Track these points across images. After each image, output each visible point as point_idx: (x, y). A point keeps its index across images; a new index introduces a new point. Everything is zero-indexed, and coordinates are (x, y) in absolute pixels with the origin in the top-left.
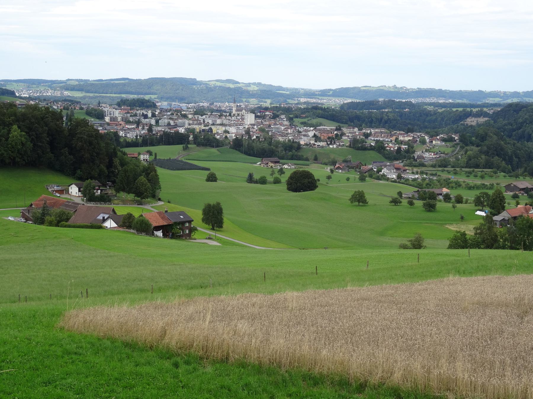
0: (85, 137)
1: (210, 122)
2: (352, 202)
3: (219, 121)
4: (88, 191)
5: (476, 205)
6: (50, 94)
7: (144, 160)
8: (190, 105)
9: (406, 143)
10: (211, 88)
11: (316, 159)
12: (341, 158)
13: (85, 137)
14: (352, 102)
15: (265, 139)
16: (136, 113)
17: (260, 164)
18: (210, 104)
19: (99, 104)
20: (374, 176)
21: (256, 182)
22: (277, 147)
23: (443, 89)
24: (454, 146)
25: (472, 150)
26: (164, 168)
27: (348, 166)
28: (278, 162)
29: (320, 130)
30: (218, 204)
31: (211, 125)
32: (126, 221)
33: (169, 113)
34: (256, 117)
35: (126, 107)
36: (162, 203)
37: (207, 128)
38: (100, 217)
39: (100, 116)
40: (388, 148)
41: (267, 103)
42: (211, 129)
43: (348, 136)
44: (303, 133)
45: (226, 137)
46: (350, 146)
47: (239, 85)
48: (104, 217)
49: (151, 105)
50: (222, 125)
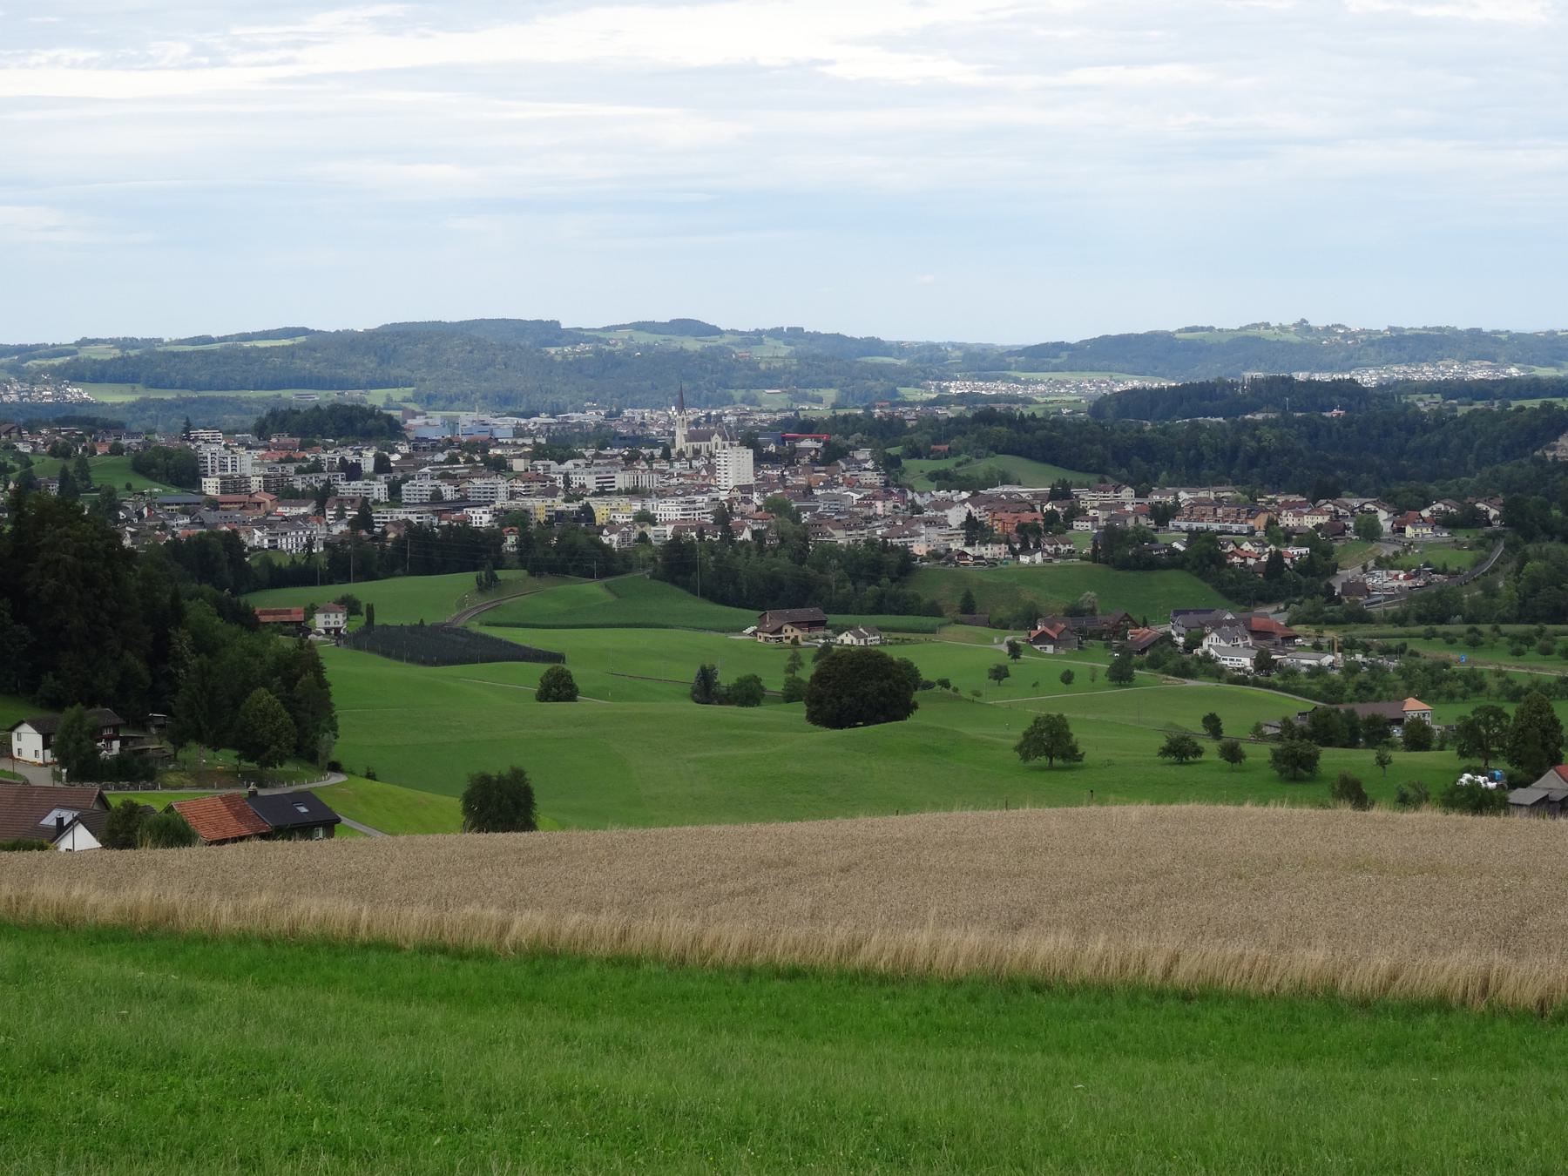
0: (70, 559)
1: (591, 483)
2: (1026, 757)
3: (622, 480)
4: (72, 745)
5: (1462, 754)
6: (15, 397)
7: (328, 630)
8: (531, 423)
9: (1306, 538)
10: (611, 353)
11: (968, 609)
12: (1057, 603)
13: (70, 559)
14: (1134, 391)
15: (783, 541)
16: (317, 461)
17: (754, 633)
18: (610, 415)
19: (187, 430)
20: (1170, 664)
21: (726, 699)
22: (821, 567)
23: (1487, 328)
24: (1481, 544)
25: (1541, 557)
26: (399, 658)
27: (1081, 631)
28: (822, 624)
29: (990, 499)
30: (518, 774)
31: (595, 494)
32: (117, 827)
33: (440, 457)
34: (761, 459)
35: (286, 439)
36: (342, 778)
37: (574, 506)
38: (50, 821)
39: (186, 473)
40: (1236, 560)
41: (822, 404)
42: (587, 510)
43: (1095, 519)
44: (929, 514)
45: (643, 537)
46: (1094, 557)
47: (721, 341)
48: (60, 821)
49: (384, 429)
50: (634, 492)
